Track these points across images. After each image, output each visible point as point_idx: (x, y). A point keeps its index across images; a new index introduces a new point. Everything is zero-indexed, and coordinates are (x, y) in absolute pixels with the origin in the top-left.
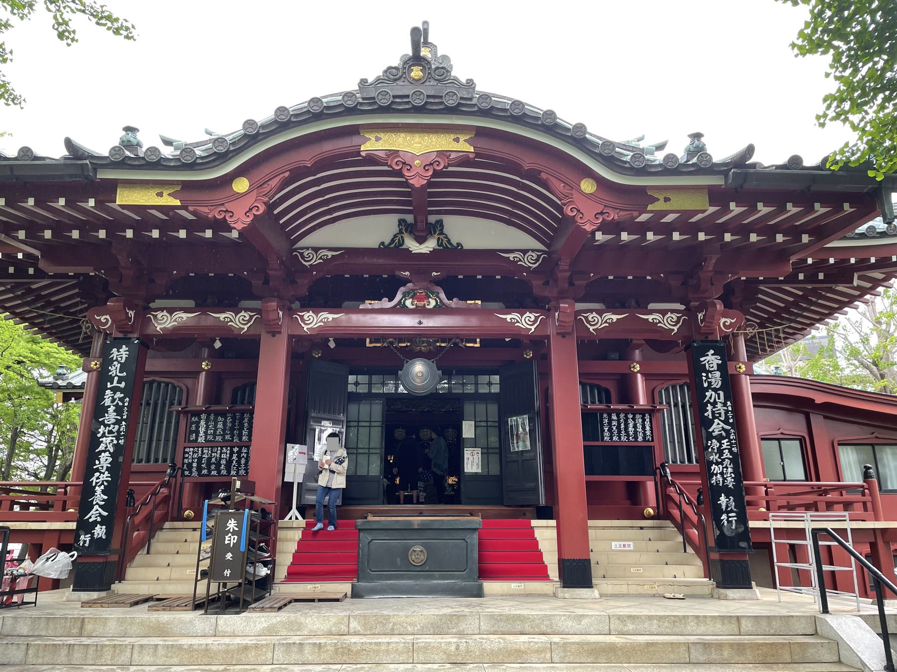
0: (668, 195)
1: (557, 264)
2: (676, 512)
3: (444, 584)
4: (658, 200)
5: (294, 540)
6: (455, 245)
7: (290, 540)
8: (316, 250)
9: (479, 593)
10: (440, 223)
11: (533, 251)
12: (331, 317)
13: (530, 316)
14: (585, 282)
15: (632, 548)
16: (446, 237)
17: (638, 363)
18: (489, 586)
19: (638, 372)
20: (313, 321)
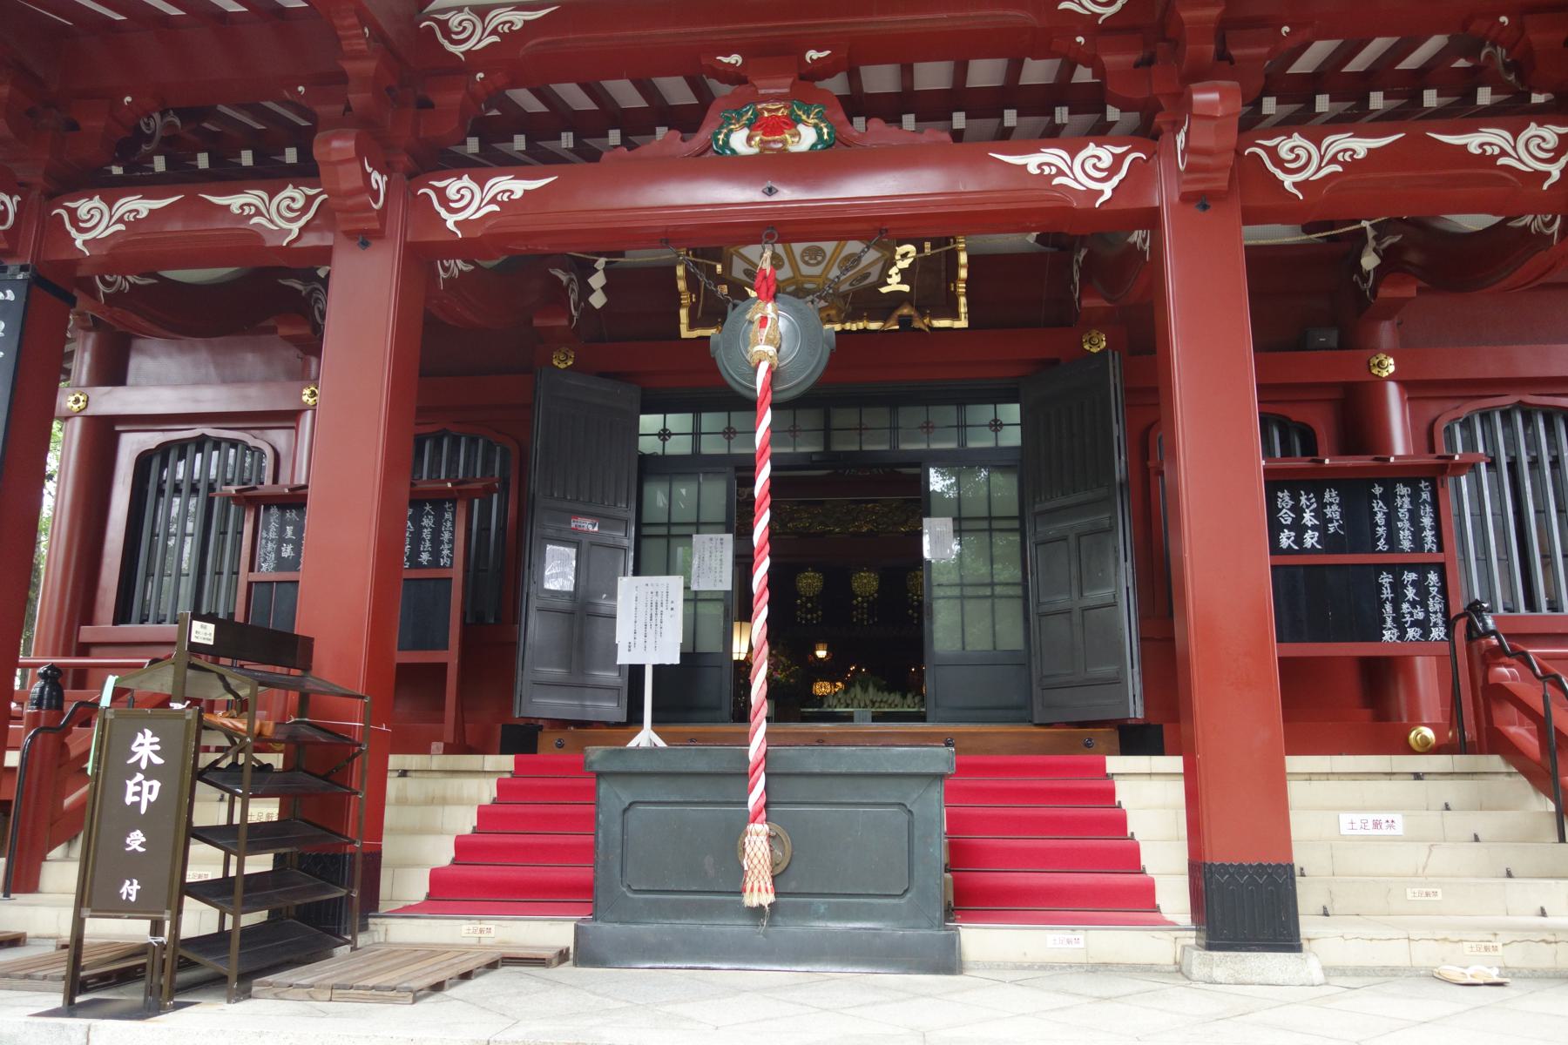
2: (1521, 733)
3: (848, 931)
5: (469, 803)
7: (459, 801)
9: (947, 962)
13: (293, 195)
15: (1399, 830)
17: (1389, 354)
18: (980, 940)
19: (1391, 377)
20: (467, 201)
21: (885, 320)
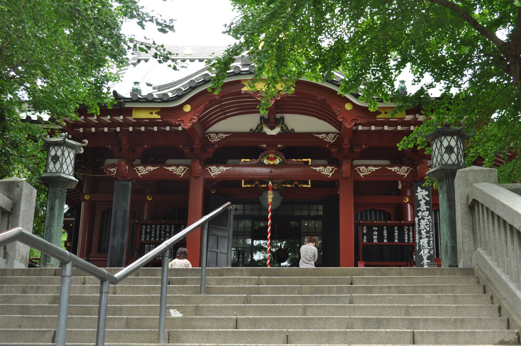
0: (386, 111)
1: (343, 141)
4: (381, 113)
6: (290, 129)
8: (217, 133)
10: (282, 118)
11: (332, 133)
12: (225, 169)
13: (405, 168)
14: (359, 150)
16: (286, 126)
19: (408, 202)
20: (215, 171)
21: (291, 185)
